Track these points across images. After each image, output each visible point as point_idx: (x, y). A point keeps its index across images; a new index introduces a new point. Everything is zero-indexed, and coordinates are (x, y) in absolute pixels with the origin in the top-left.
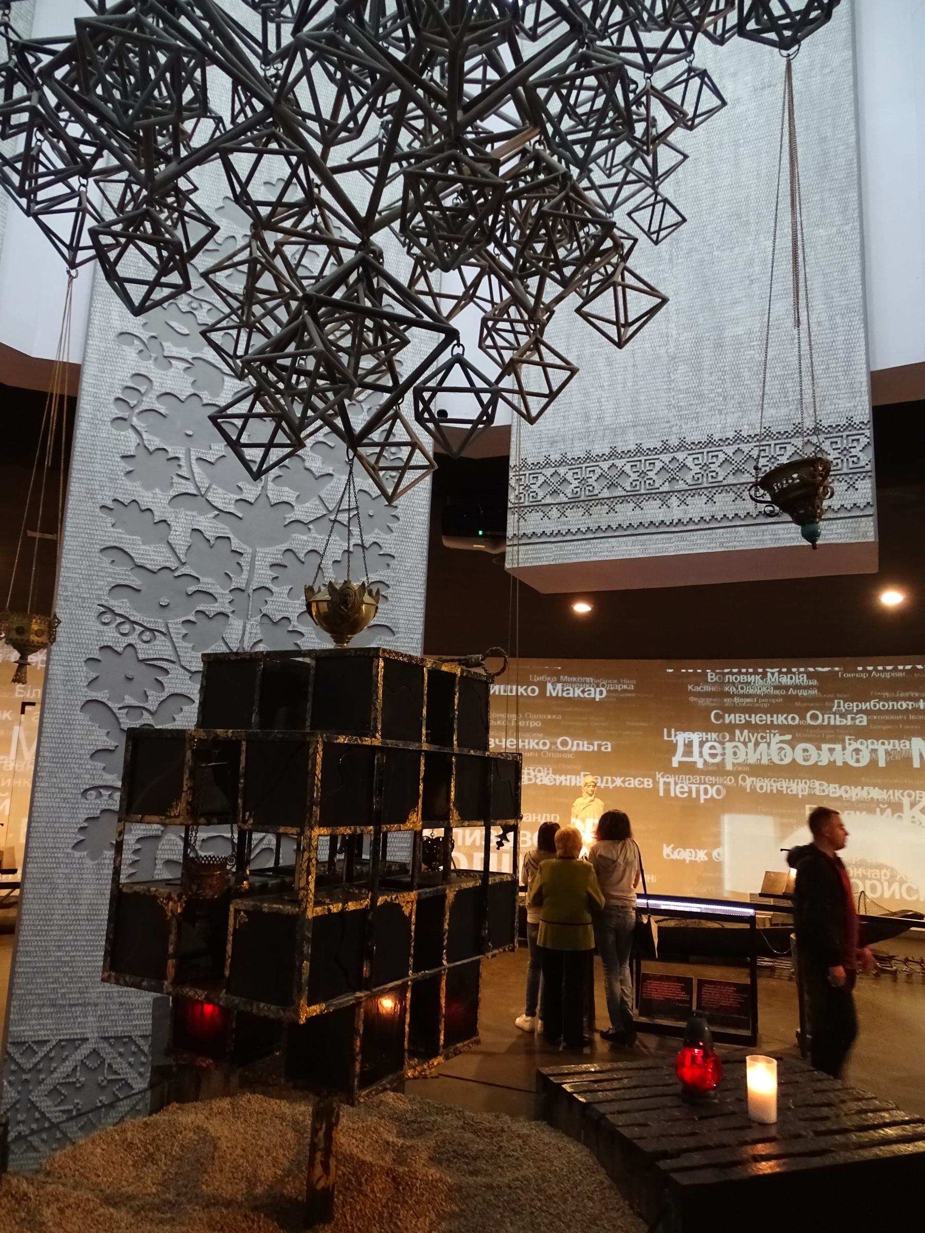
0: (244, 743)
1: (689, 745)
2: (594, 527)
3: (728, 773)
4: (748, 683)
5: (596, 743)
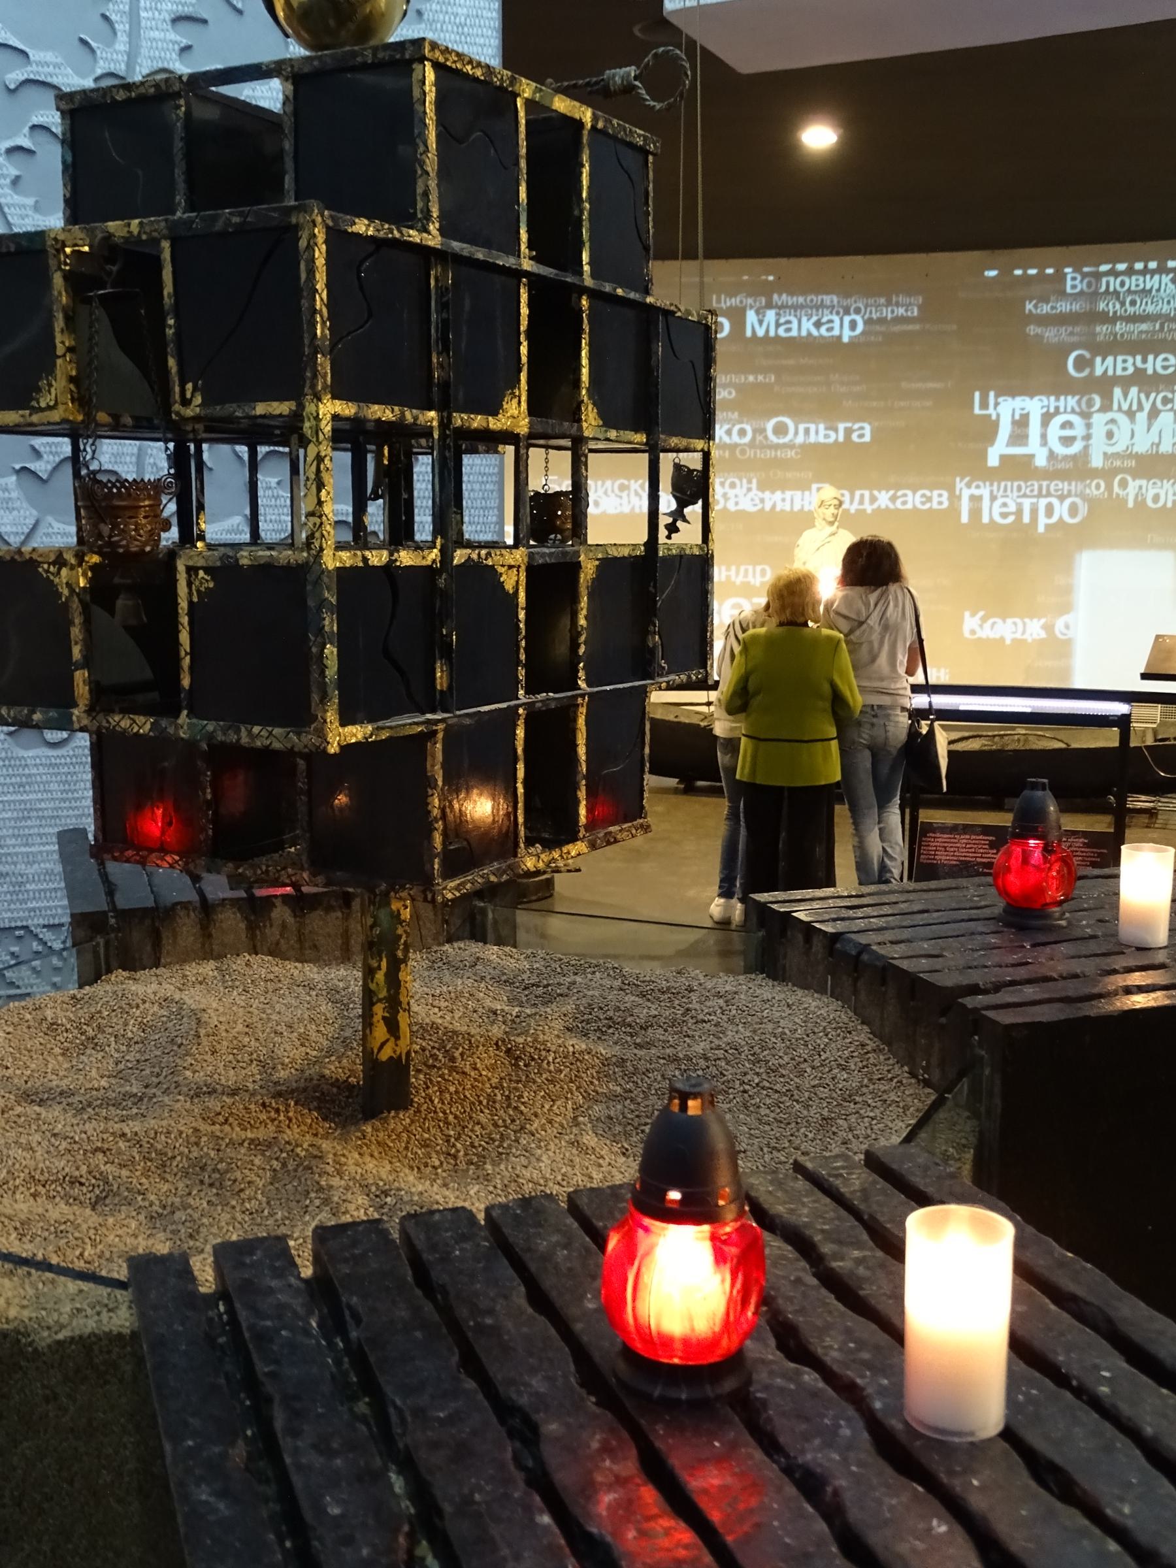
0: (166, 245)
1: (1021, 423)
3: (1095, 473)
4: (1146, 292)
5: (841, 427)
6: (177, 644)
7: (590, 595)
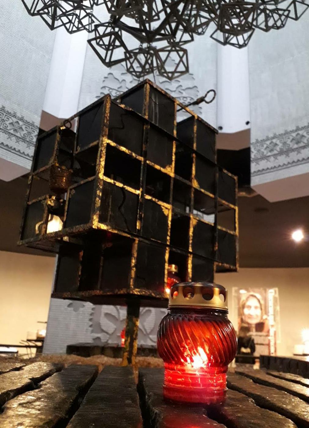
2: (291, 161)
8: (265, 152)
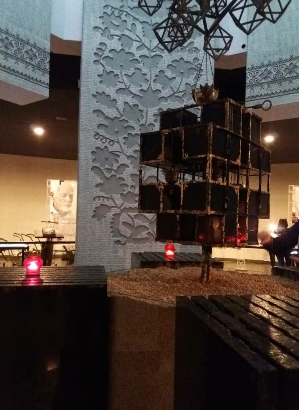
6: (180, 197)
7: (249, 197)
8: (260, 79)
